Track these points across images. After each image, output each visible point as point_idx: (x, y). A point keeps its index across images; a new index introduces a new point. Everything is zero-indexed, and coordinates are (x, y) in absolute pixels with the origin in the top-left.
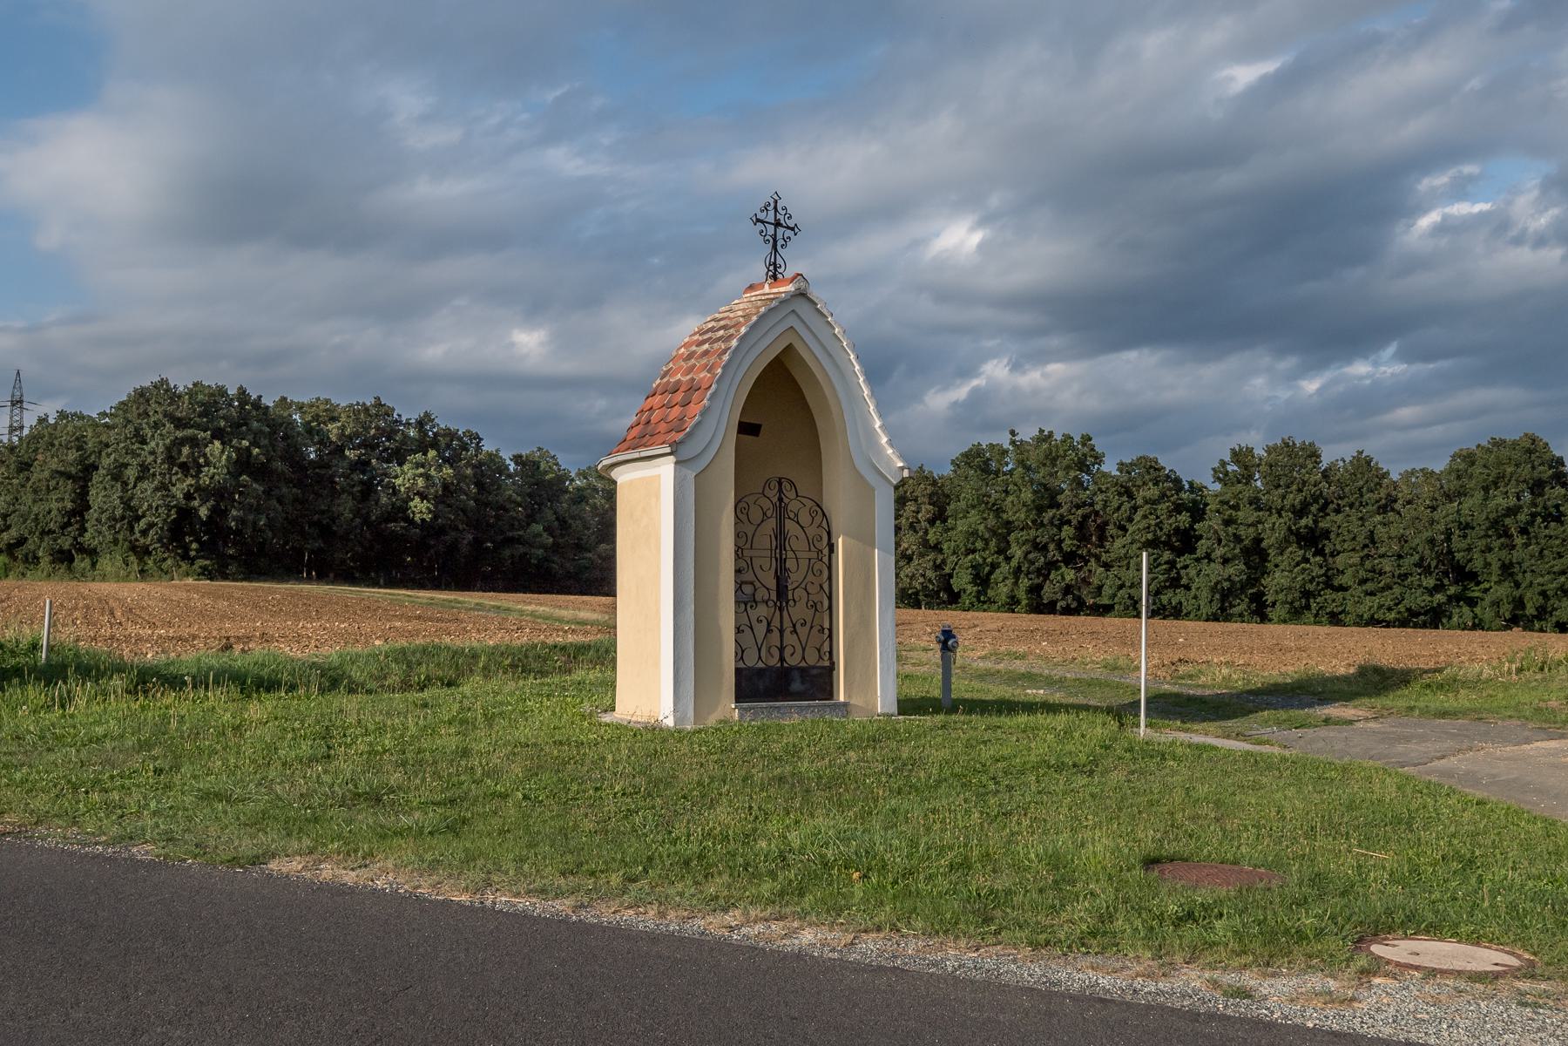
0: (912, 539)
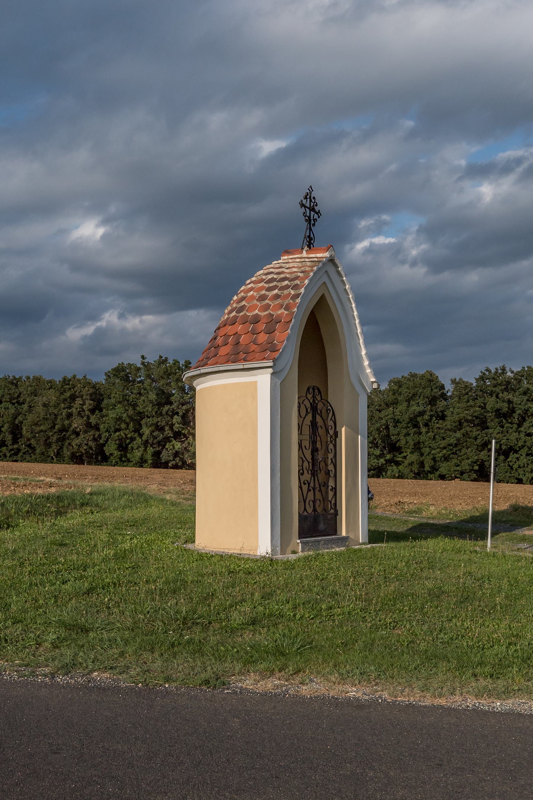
0: (80, 422)
